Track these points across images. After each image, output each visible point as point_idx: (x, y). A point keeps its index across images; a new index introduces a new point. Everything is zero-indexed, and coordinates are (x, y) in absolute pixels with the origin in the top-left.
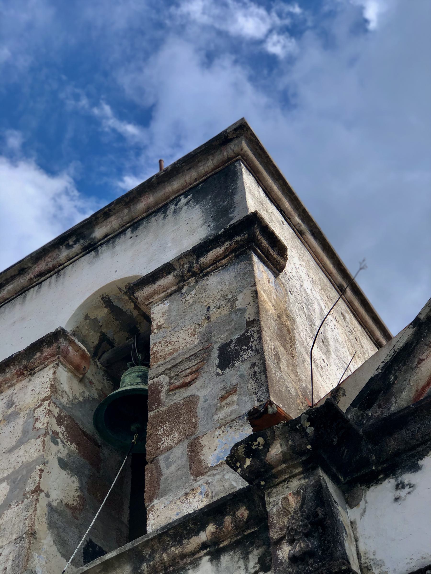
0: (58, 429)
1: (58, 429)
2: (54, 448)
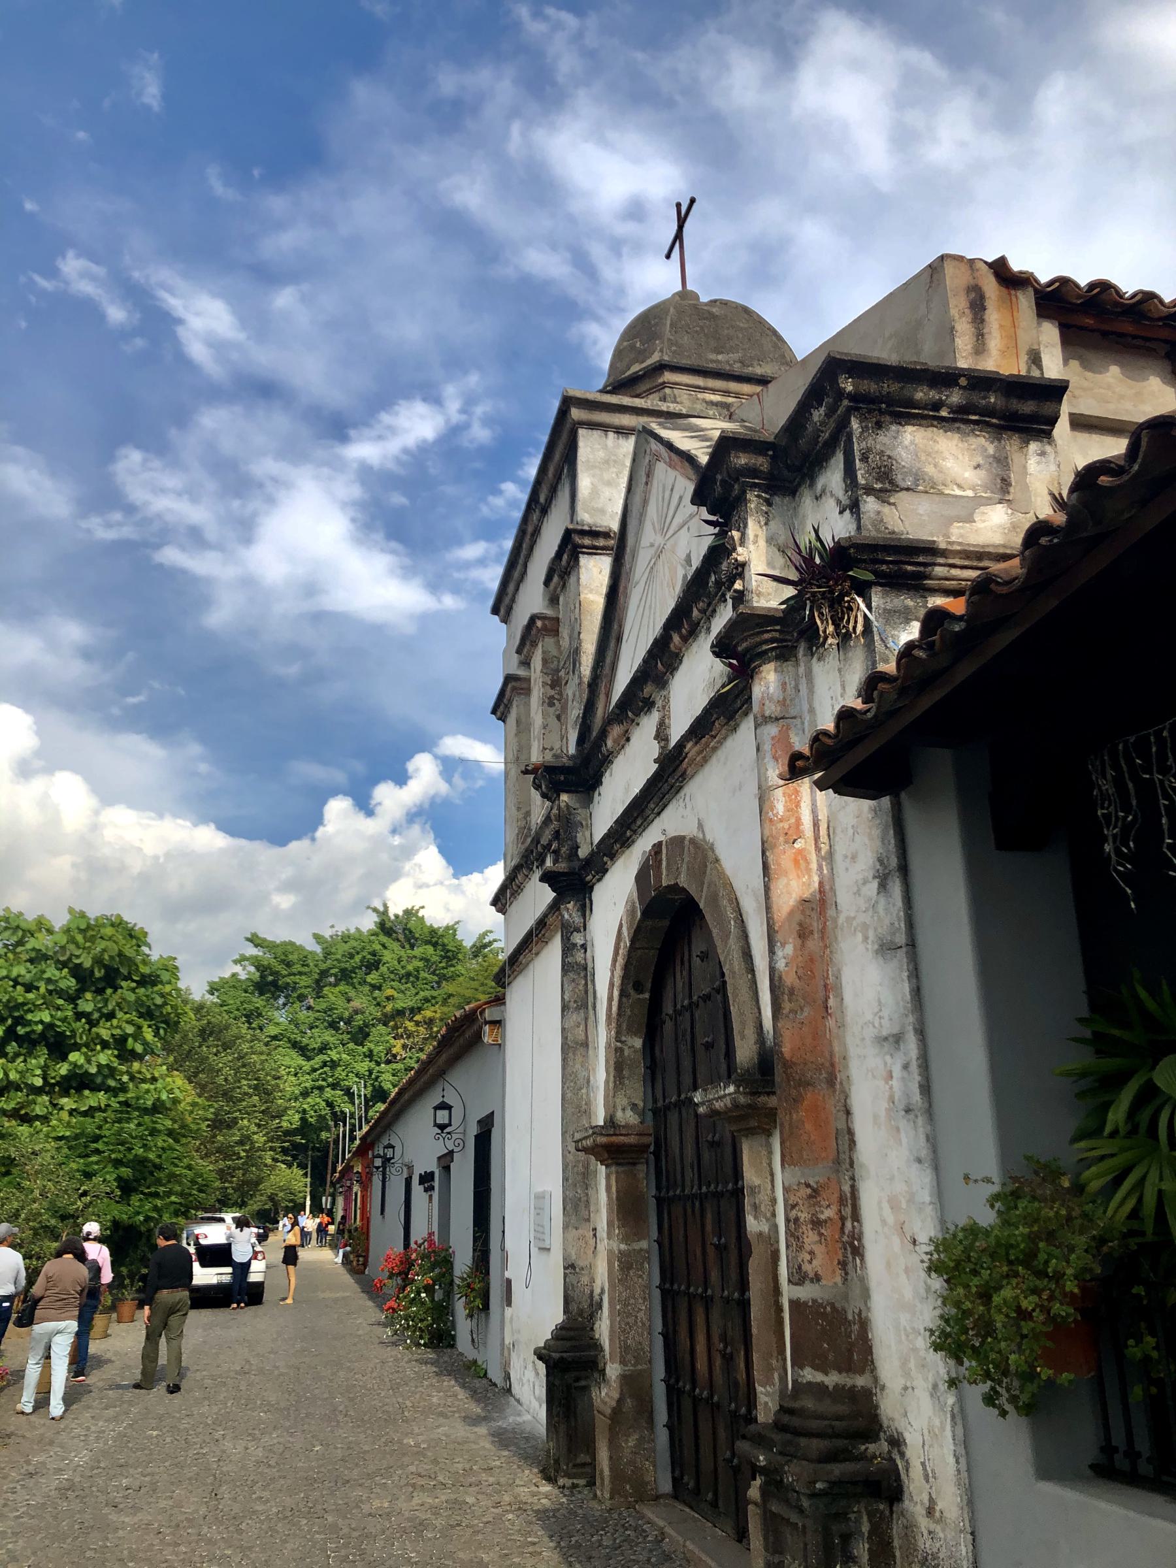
0: (552, 693)
1: (552, 693)
2: (552, 710)
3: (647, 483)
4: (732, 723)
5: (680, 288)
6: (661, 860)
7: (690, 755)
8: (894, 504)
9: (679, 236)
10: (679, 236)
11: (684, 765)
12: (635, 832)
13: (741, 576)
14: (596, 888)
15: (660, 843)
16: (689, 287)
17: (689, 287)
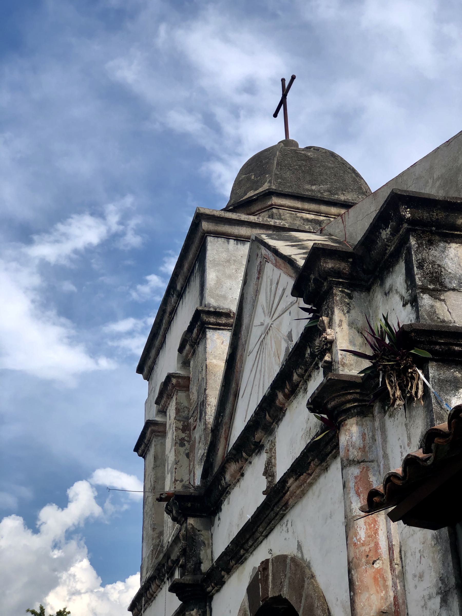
0: (183, 435)
1: (183, 435)
2: (182, 449)
3: (258, 278)
4: (324, 464)
5: (284, 138)
6: (268, 575)
7: (291, 489)
8: (444, 300)
9: (283, 102)
10: (283, 102)
11: (287, 497)
12: (247, 551)
13: (330, 350)
14: (215, 597)
15: (267, 560)
16: (291, 138)
17: (291, 138)
